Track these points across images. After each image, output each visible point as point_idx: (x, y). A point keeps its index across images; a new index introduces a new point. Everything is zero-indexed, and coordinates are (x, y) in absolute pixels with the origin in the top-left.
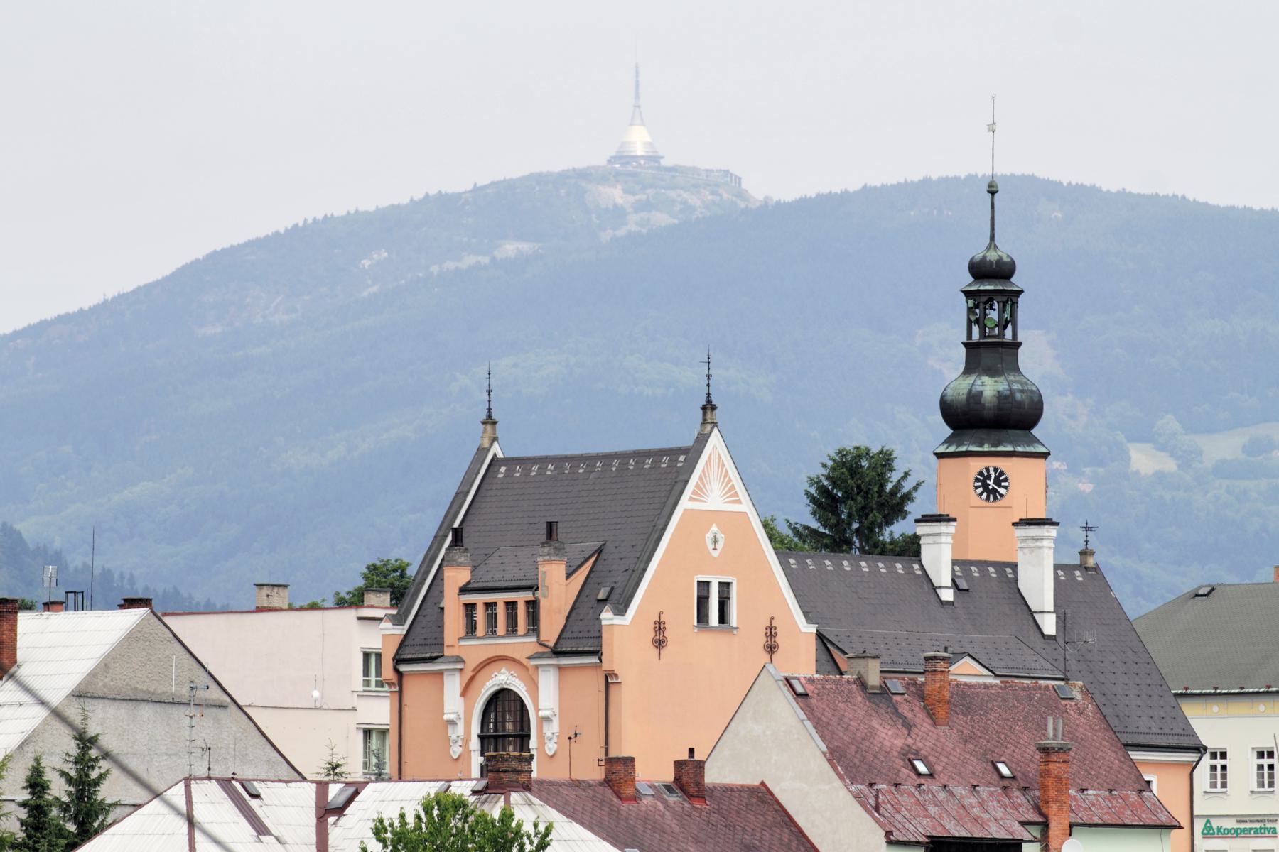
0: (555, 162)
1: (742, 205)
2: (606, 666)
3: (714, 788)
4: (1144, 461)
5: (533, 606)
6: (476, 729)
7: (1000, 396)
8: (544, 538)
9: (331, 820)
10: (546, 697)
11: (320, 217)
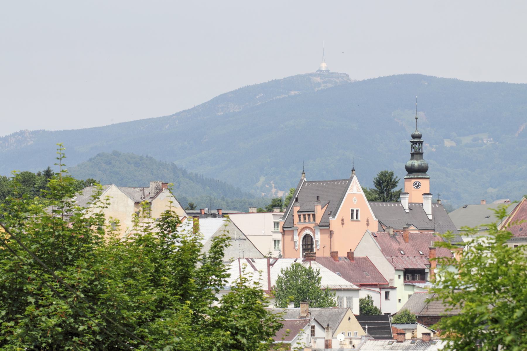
0: (303, 72)
1: (349, 82)
2: (330, 229)
3: (356, 258)
4: (448, 143)
5: (314, 216)
7: (419, 165)
8: (316, 200)
9: (271, 267)
10: (318, 237)
11: (246, 86)
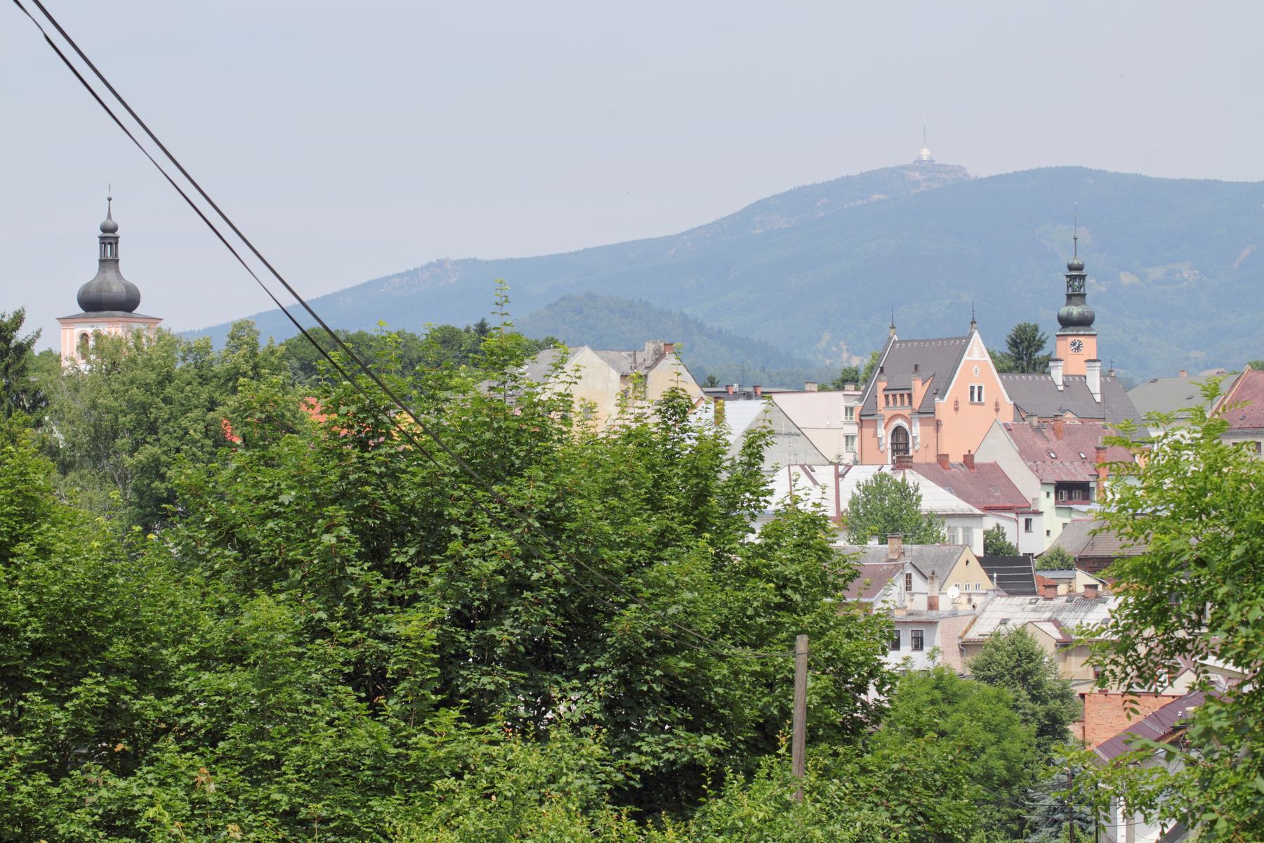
5: (910, 396)
6: (889, 441)
7: (1080, 314)
10: (916, 430)
